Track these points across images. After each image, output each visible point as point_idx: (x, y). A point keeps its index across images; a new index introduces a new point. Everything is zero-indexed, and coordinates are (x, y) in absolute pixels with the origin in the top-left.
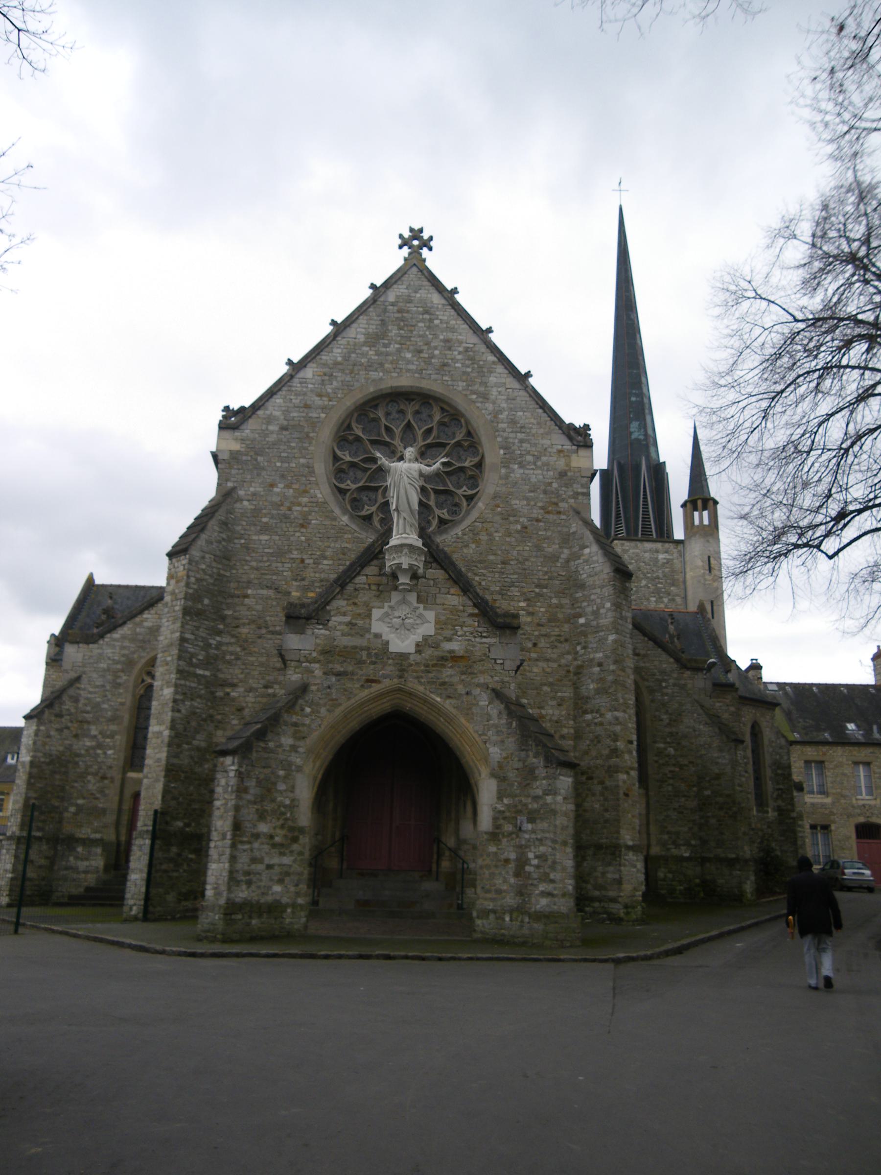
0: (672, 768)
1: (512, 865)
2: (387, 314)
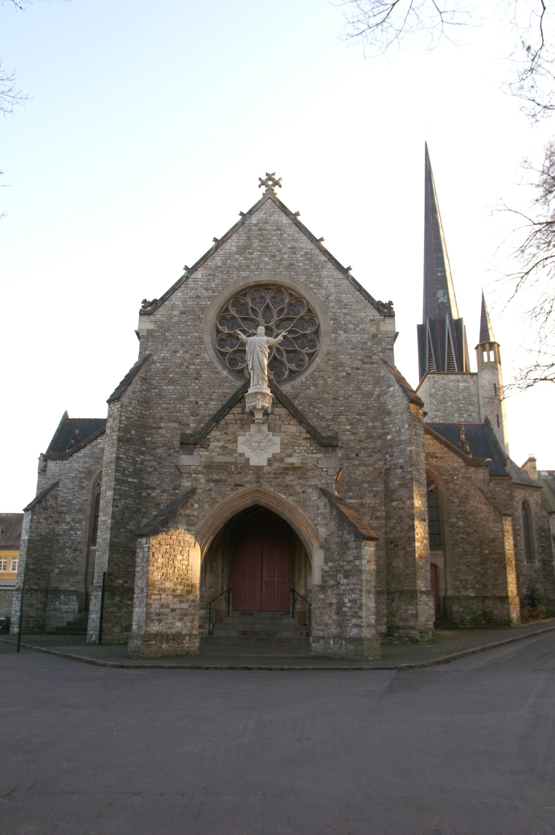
0: (462, 536)
1: (334, 607)
2: (251, 232)
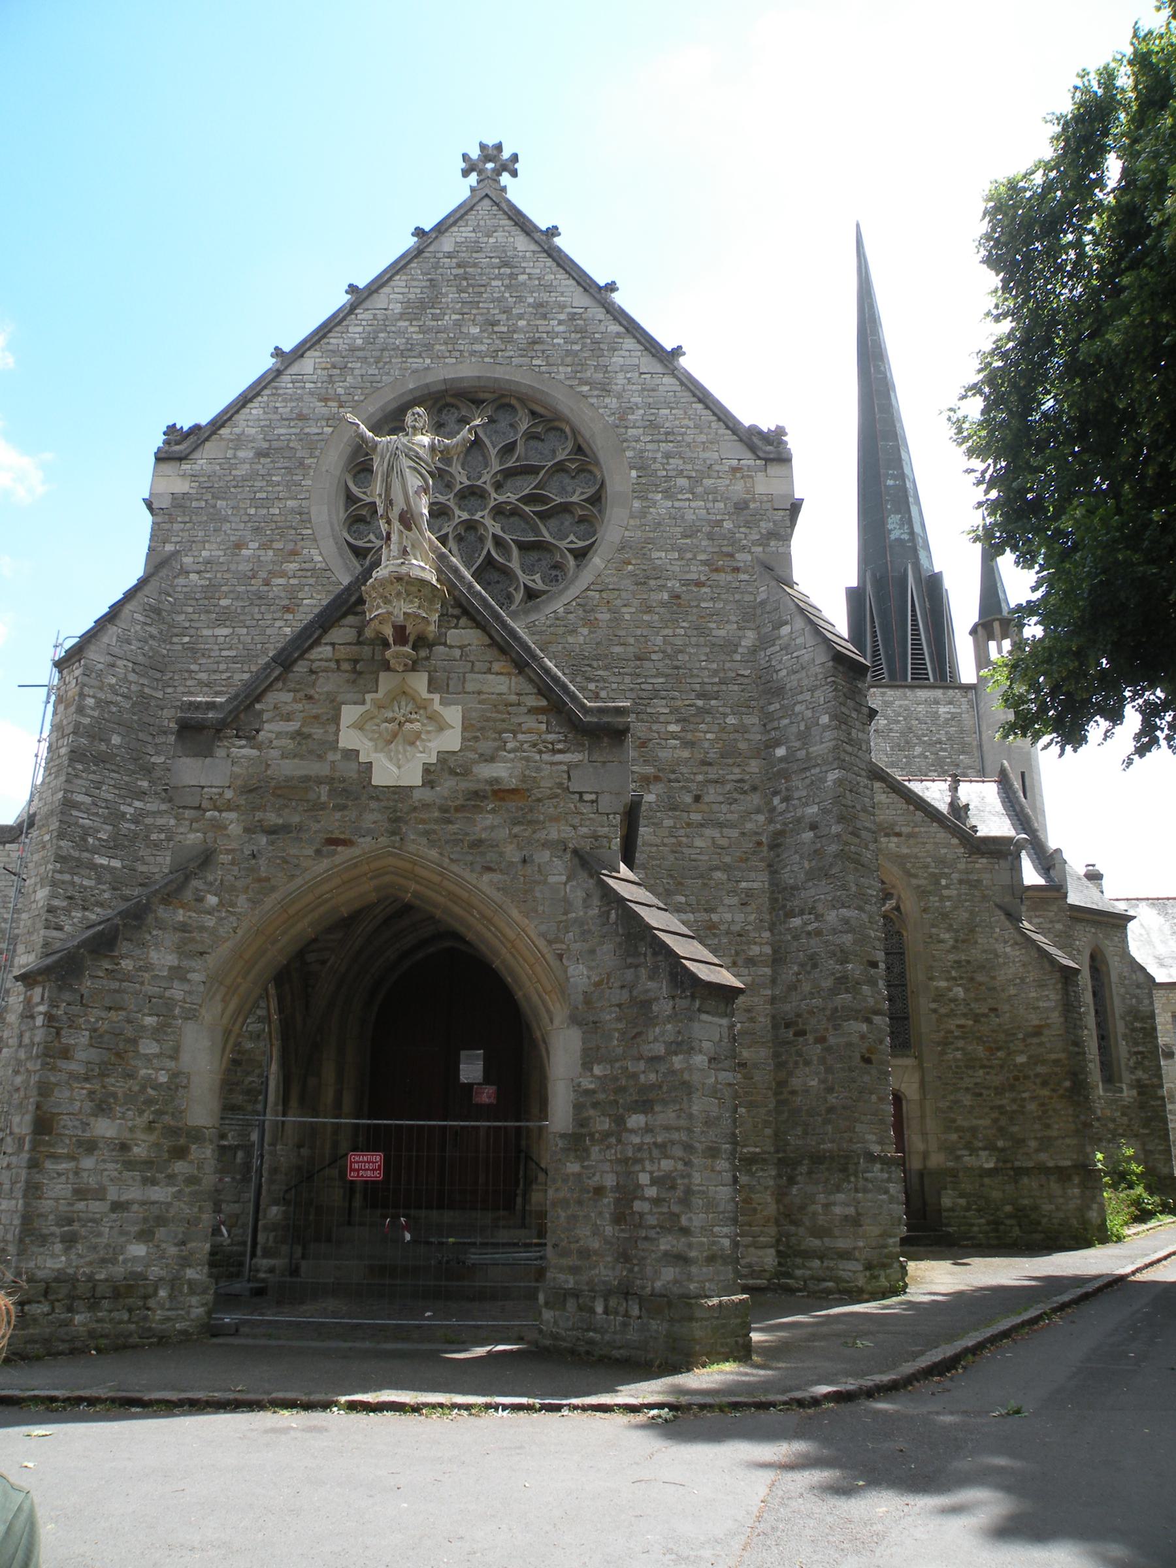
0: (962, 1022)
1: (608, 1200)
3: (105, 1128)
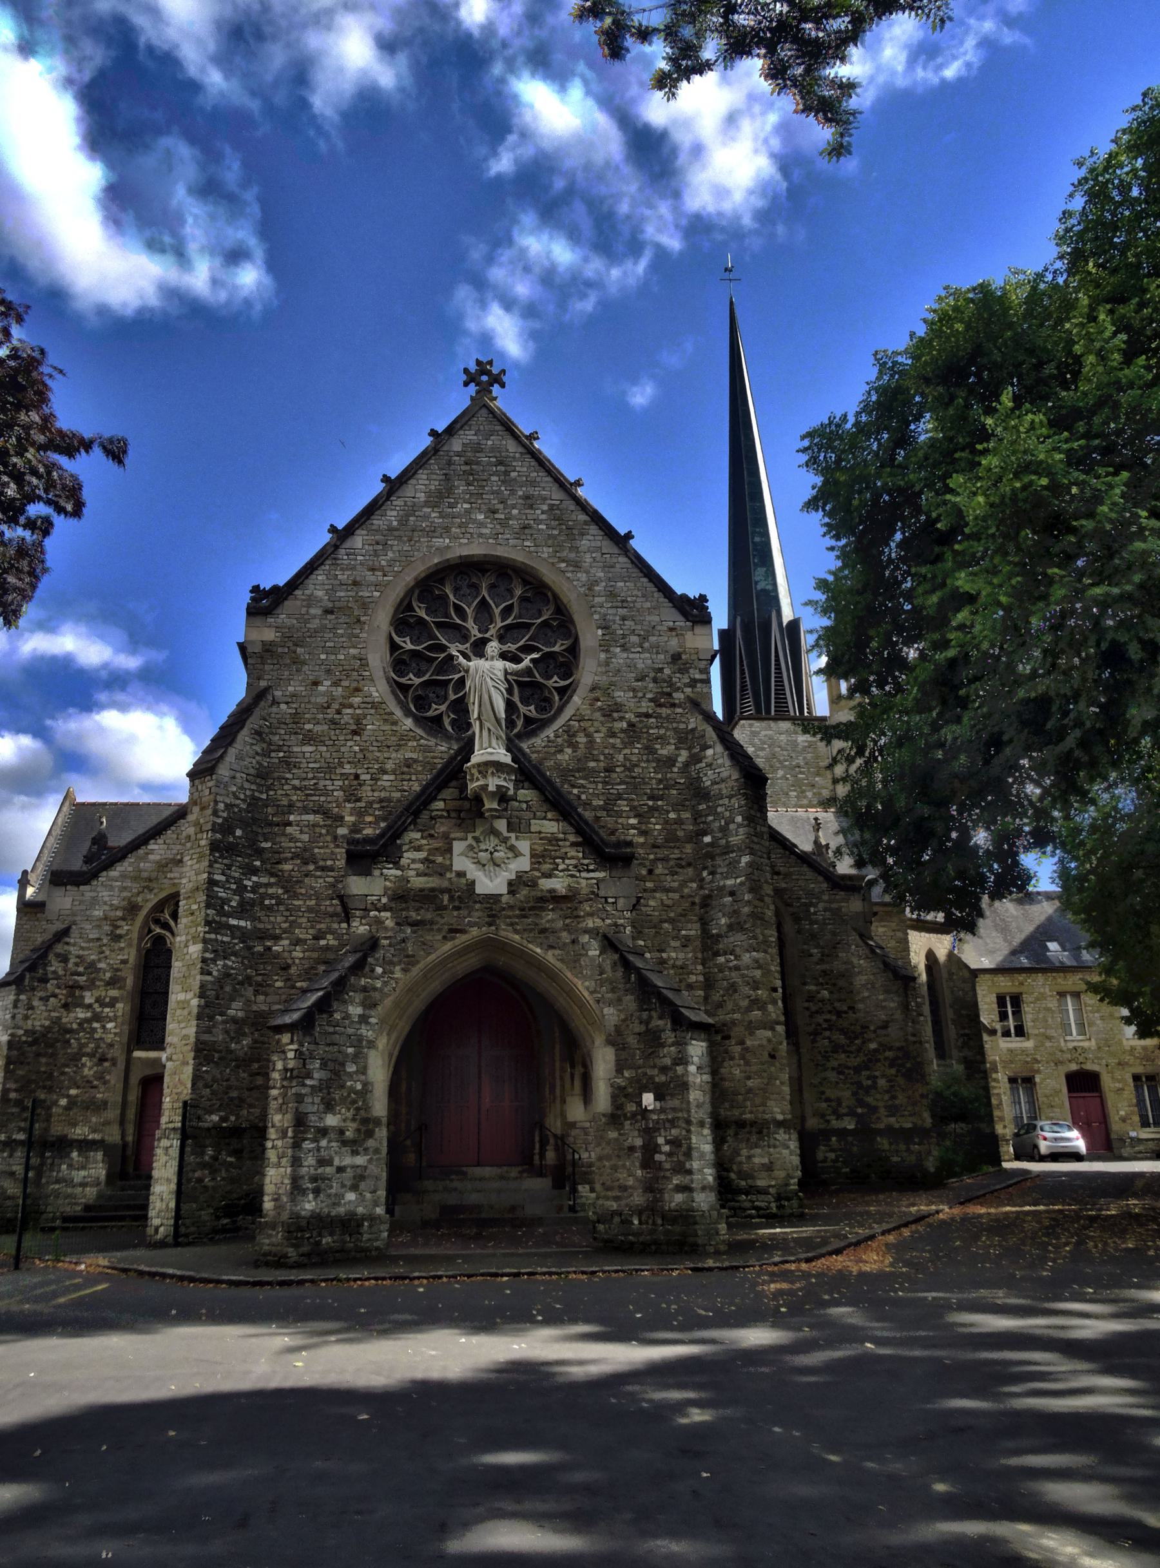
0: (828, 1017)
1: (638, 1154)
2: (453, 467)
3: (331, 1120)
